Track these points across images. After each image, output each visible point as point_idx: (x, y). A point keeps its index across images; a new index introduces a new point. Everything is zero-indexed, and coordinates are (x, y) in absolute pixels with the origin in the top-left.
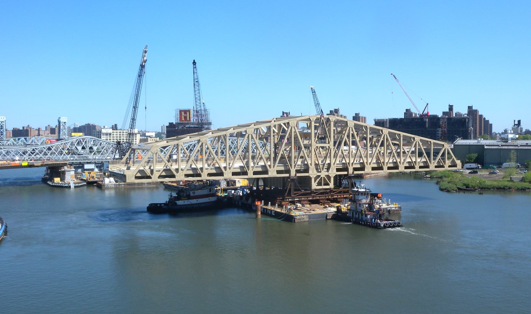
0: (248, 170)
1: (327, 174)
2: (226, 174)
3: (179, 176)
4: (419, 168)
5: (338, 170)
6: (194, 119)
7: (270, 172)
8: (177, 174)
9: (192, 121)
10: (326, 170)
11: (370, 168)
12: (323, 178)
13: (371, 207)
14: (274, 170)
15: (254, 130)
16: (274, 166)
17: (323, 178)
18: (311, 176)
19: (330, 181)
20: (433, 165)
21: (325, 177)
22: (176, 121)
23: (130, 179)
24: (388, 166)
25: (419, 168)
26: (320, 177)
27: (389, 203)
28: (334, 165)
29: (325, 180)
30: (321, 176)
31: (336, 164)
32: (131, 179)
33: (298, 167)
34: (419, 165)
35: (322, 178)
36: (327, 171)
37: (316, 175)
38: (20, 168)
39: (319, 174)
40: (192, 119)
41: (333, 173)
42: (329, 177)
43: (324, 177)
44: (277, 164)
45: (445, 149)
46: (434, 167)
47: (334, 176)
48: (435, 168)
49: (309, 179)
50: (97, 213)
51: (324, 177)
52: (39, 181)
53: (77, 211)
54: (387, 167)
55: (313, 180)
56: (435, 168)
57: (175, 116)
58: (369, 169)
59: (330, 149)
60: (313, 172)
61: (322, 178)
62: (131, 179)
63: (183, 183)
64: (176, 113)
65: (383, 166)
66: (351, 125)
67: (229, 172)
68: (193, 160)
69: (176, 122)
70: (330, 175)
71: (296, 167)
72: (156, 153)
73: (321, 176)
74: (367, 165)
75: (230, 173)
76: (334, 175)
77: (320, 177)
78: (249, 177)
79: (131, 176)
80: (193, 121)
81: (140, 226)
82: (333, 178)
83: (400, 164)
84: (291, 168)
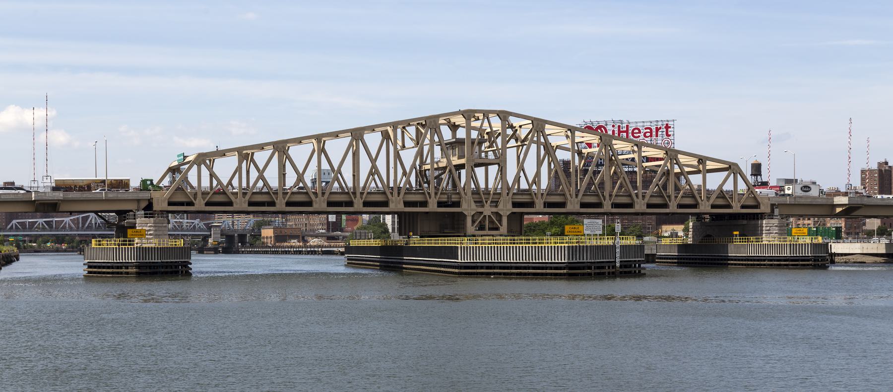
1: (494, 210)
8: (315, 199)
11: (644, 205)
12: (487, 216)
14: (400, 200)
17: (487, 216)
18: (466, 213)
19: (500, 221)
20: (707, 203)
23: (160, 204)
28: (398, 196)
29: (491, 222)
30: (484, 214)
31: (511, 194)
35: (485, 216)
37: (511, 212)
38: (430, 299)
39: (480, 210)
42: (498, 215)
49: (461, 216)
51: (489, 216)
52: (73, 279)
55: (469, 220)
58: (322, 203)
60: (469, 205)
61: (485, 216)
65: (669, 202)
68: (630, 125)
70: (501, 213)
73: (484, 214)
76: (508, 213)
77: (483, 215)
79: (161, 200)
81: (273, 268)
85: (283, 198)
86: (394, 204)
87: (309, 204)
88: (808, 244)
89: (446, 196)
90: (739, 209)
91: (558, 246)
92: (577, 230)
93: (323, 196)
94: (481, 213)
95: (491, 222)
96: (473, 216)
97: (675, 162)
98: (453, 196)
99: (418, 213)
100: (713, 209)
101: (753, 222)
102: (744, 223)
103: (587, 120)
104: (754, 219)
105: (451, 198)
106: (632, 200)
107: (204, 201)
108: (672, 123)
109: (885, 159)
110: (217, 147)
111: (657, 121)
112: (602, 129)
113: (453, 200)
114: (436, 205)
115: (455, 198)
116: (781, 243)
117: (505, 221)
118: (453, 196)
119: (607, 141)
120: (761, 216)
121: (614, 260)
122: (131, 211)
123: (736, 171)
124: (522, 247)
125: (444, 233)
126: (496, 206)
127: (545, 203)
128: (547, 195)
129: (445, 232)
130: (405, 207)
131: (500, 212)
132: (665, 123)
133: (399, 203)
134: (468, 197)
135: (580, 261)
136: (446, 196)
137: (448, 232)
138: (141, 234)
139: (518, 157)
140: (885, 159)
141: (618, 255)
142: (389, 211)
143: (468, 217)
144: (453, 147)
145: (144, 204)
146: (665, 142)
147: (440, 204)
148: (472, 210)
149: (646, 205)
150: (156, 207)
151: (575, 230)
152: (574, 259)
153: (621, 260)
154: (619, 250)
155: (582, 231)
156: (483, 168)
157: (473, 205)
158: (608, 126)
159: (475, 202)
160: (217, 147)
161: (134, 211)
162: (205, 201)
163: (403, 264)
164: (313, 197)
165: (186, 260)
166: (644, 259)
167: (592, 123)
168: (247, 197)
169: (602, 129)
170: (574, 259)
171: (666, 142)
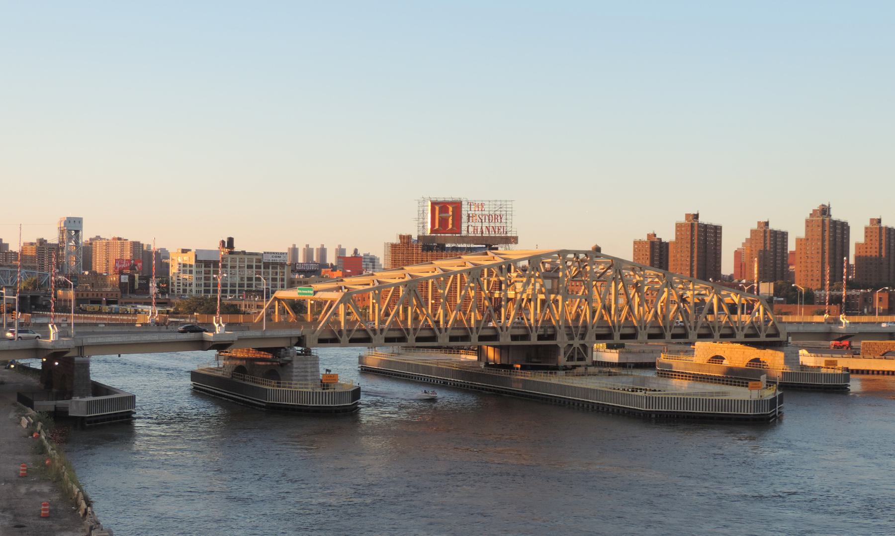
1: (582, 342)
4: (416, 342)
6: (470, 227)
9: (464, 233)
12: (576, 348)
13: (559, 378)
17: (576, 348)
20: (742, 333)
21: (580, 348)
22: (419, 231)
26: (573, 348)
30: (574, 346)
34: (720, 332)
39: (571, 342)
40: (464, 227)
48: (479, 340)
51: (578, 348)
53: (858, 395)
54: (671, 334)
55: (562, 351)
56: (479, 340)
57: (417, 217)
61: (575, 348)
64: (419, 211)
69: (421, 234)
73: (574, 346)
74: (691, 330)
77: (573, 348)
78: (501, 344)
80: (468, 231)
83: (738, 331)
84: (615, 331)
85: (347, 335)
87: (433, 338)
90: (764, 337)
93: (381, 334)
94: (571, 345)
97: (619, 277)
98: (549, 330)
100: (747, 339)
106: (636, 331)
108: (510, 203)
109: (698, 211)
111: (496, 201)
115: (550, 332)
116: (682, 397)
118: (549, 330)
122: (283, 348)
124: (285, 402)
128: (651, 327)
130: (512, 340)
131: (586, 344)
132: (499, 203)
140: (698, 211)
143: (589, 349)
147: (540, 338)
149: (647, 336)
151: (331, 378)
157: (566, 338)
159: (567, 334)
161: (286, 348)
162: (349, 338)
164: (437, 332)
165: (129, 410)
168: (384, 334)
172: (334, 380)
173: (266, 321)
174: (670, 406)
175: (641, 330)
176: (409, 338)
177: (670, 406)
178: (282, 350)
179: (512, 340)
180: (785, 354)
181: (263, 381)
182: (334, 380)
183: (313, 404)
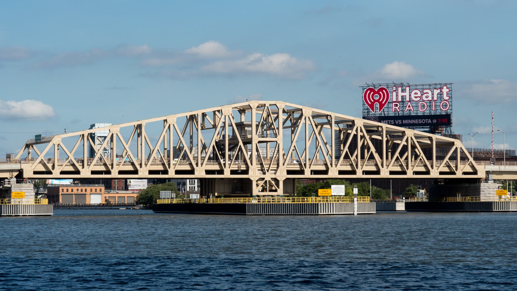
0: (357, 169)
1: (274, 176)
2: (141, 172)
3: (142, 171)
4: (119, 174)
5: (289, 172)
7: (197, 171)
10: (273, 172)
11: (387, 172)
14: (203, 169)
15: (275, 104)
16: (202, 164)
23: (28, 173)
24: (231, 169)
25: (119, 174)
26: (264, 181)
27: (247, 214)
29: (271, 185)
32: (29, 173)
33: (234, 166)
34: (175, 169)
36: (275, 173)
39: (263, 176)
41: (282, 175)
42: (277, 181)
43: (269, 181)
44: (94, 161)
45: (457, 148)
46: (437, 173)
47: (283, 180)
48: (119, 174)
49: (249, 182)
50: (385, 281)
51: (269, 181)
56: (119, 174)
58: (386, 173)
59: (278, 144)
61: (266, 181)
62: (29, 173)
63: (430, 193)
66: (307, 113)
67: (145, 170)
71: (232, 166)
72: (58, 144)
75: (146, 171)
82: (282, 182)
83: (332, 166)
86: (198, 172)
88: (23, 205)
89: (237, 166)
91: (300, 204)
92: (327, 193)
94: (263, 179)
95: (271, 185)
96: (257, 181)
99: (215, 179)
101: (473, 185)
102: (466, 186)
103: (370, 83)
104: (474, 183)
105: (241, 167)
107: (59, 170)
110: (65, 129)
112: (384, 91)
113: (242, 169)
114: (229, 172)
117: (281, 184)
119: (359, 123)
120: (479, 180)
121: (353, 213)
122: (7, 178)
123: (458, 146)
125: (235, 194)
126: (275, 173)
127: (312, 171)
129: (236, 193)
130: (206, 174)
133: (202, 172)
134: (253, 167)
135: (321, 214)
136: (237, 166)
137: (238, 193)
138: (21, 195)
139: (279, 155)
141: (356, 210)
142: (194, 177)
144: (242, 128)
145: (15, 174)
146: (443, 104)
148: (256, 176)
150: (25, 175)
151: (325, 192)
152: (325, 212)
153: (358, 213)
154: (356, 206)
155: (330, 193)
156: (266, 143)
158: (389, 88)
160: (65, 129)
163: (368, 150)
166: (375, 213)
167: (374, 86)
169: (384, 91)
170: (325, 212)
171: (444, 104)
172: (21, 196)
173: (437, 152)
174: (325, 210)
175: (332, 166)
176: (357, 171)
177: (325, 210)
178: (6, 180)
179: (206, 174)
180: (345, 185)
181: (363, 198)
182: (21, 196)
183: (496, 209)
